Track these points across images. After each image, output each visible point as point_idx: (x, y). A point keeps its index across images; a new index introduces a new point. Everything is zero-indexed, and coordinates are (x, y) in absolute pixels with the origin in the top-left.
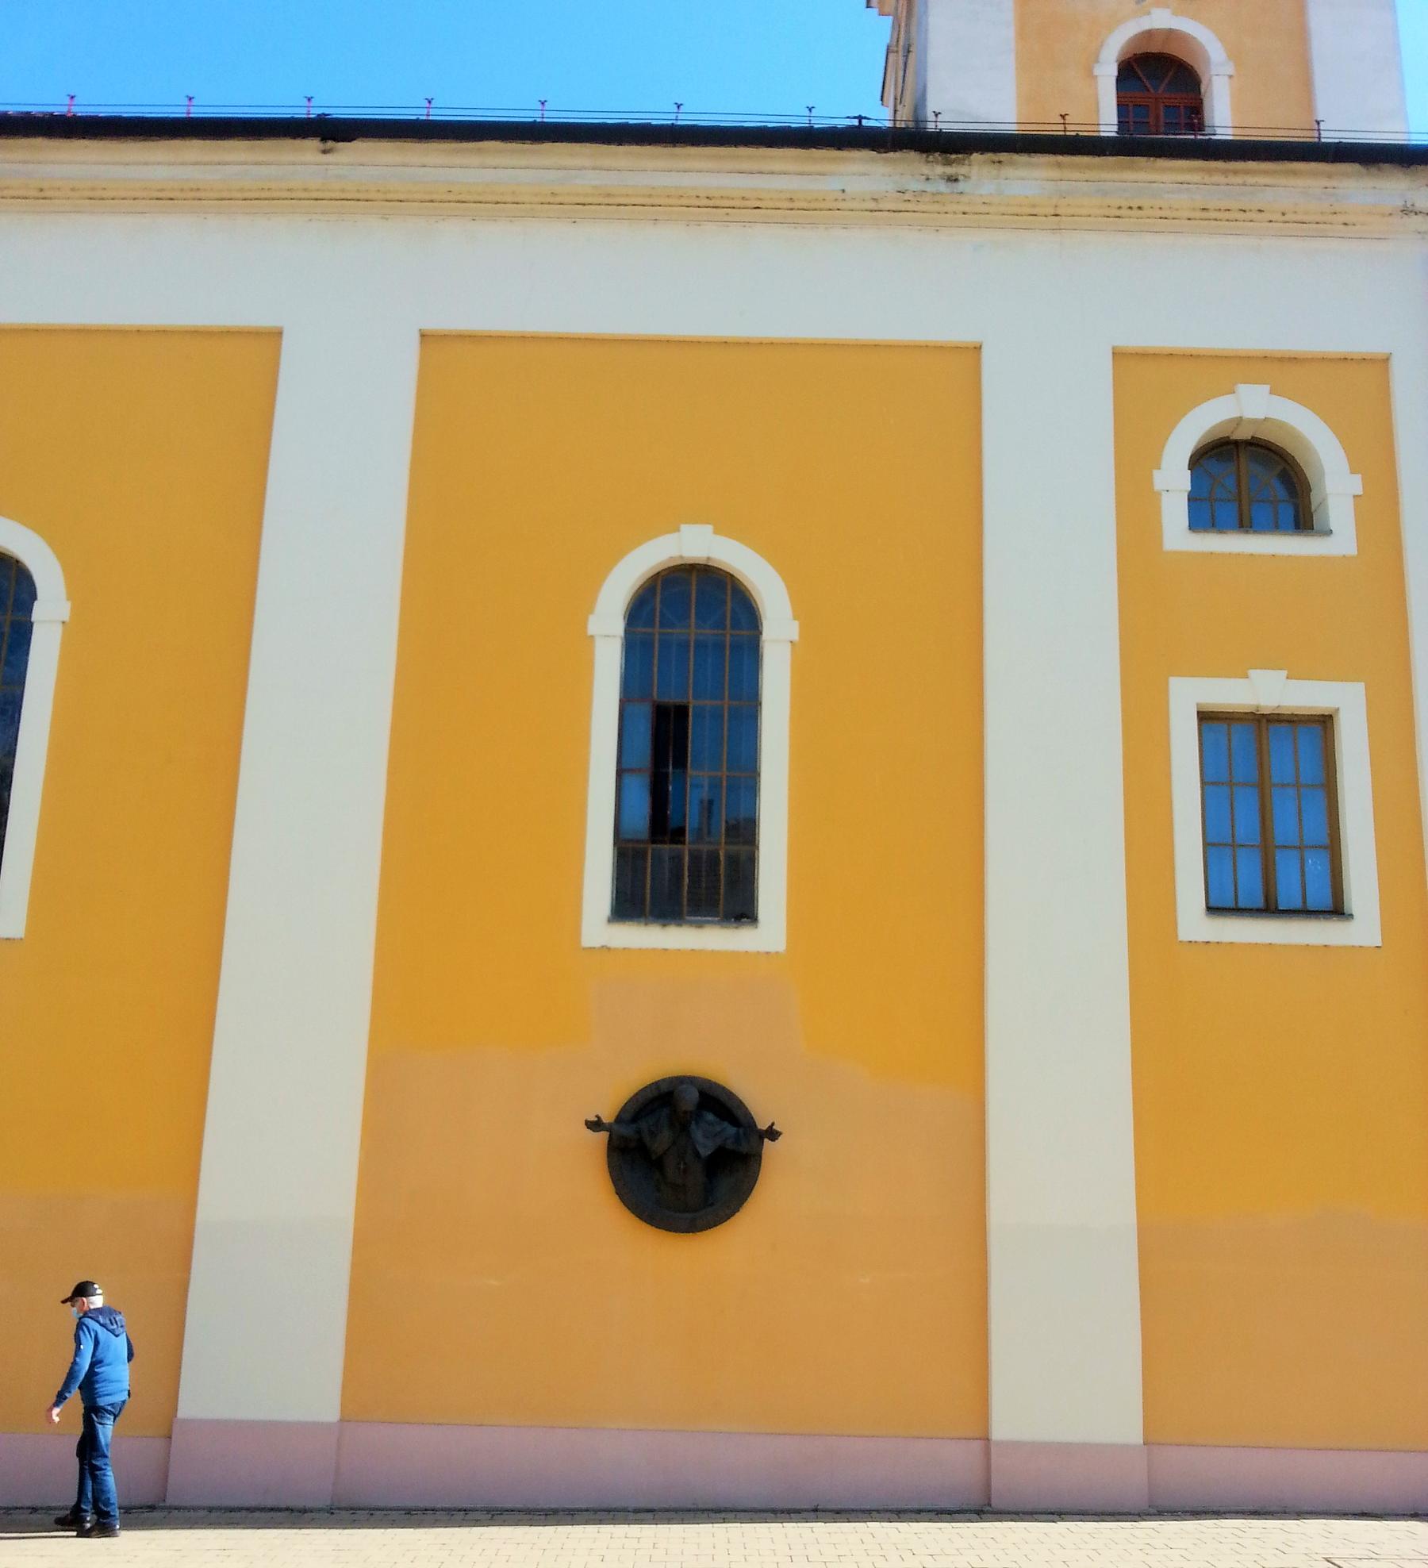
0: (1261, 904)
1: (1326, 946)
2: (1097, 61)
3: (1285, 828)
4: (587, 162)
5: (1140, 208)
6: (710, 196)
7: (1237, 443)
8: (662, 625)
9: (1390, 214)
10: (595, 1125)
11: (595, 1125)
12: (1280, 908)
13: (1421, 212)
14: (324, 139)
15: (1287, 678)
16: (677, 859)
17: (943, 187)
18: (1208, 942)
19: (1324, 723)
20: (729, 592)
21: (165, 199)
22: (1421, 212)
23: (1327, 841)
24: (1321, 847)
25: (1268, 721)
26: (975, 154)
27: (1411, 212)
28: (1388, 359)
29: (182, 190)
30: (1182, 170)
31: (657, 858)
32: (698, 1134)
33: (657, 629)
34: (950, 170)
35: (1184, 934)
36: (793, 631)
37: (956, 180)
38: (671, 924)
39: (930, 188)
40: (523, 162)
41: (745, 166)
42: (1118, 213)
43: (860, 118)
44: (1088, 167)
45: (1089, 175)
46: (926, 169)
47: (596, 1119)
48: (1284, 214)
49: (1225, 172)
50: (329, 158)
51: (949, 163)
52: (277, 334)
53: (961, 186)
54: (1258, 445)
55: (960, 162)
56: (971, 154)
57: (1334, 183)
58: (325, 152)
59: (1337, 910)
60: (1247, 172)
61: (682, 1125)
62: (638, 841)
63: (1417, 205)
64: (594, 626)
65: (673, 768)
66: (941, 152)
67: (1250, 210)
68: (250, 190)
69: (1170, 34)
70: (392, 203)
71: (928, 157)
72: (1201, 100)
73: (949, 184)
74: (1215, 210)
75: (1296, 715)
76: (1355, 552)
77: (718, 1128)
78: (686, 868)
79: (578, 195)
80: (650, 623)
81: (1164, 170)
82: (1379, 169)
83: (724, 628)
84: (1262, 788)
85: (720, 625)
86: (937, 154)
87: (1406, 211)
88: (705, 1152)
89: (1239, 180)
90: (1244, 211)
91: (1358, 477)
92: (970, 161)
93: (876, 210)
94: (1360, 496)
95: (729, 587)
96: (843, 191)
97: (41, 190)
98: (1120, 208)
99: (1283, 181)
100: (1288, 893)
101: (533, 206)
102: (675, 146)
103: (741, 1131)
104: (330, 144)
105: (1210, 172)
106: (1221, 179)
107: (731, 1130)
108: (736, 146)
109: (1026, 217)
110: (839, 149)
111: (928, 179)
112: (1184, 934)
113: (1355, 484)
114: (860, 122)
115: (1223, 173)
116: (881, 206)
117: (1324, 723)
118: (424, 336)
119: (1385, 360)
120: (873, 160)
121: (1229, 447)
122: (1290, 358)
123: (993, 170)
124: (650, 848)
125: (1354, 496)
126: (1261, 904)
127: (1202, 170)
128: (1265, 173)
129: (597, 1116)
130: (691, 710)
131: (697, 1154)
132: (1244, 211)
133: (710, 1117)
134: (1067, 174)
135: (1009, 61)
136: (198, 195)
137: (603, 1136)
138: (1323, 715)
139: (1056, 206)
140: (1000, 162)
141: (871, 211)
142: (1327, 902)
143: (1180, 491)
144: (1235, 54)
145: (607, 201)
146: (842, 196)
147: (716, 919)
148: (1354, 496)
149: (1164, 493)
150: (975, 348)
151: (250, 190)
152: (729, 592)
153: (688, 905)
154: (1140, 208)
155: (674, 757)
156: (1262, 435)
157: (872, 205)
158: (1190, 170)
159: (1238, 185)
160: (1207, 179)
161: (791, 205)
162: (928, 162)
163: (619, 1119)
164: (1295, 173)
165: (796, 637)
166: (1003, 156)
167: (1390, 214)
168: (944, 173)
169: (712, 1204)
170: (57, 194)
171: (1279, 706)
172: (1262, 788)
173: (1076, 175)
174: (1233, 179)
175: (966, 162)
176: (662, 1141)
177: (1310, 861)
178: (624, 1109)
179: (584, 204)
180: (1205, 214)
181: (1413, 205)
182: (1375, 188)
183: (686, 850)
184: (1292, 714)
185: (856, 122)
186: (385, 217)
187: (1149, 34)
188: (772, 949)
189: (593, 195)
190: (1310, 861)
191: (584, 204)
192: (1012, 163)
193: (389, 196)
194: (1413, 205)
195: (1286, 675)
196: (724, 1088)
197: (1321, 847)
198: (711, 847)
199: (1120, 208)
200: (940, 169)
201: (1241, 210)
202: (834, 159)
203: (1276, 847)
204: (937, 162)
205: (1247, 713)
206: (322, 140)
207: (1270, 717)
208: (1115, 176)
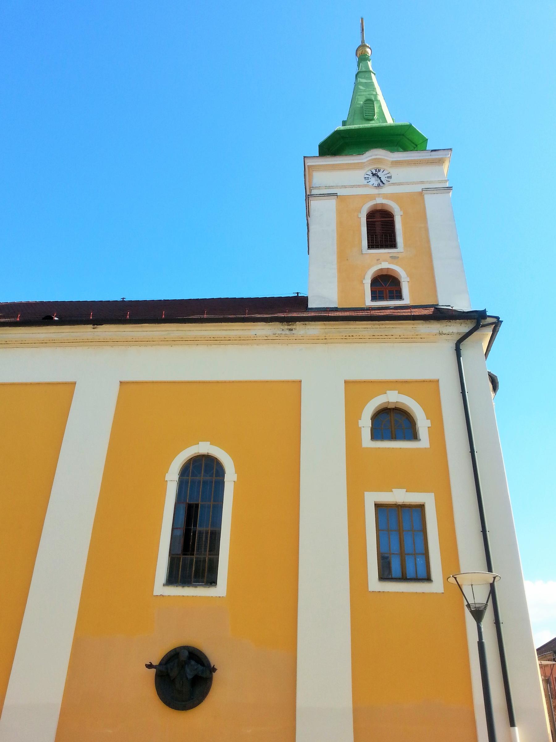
0: (400, 576)
1: (423, 593)
2: (364, 279)
3: (408, 547)
4: (175, 329)
5: (352, 336)
6: (214, 337)
7: (390, 409)
8: (192, 476)
9: (436, 335)
10: (150, 666)
11: (150, 666)
12: (408, 578)
13: (446, 334)
14: (94, 325)
15: (406, 492)
16: (192, 560)
17: (288, 332)
18: (380, 592)
19: (421, 507)
20: (215, 463)
21: (44, 343)
22: (446, 334)
23: (424, 552)
24: (422, 554)
25: (401, 507)
26: (297, 322)
27: (442, 334)
28: (438, 381)
29: (49, 340)
30: (364, 324)
31: (184, 560)
32: (188, 670)
33: (190, 478)
34: (289, 327)
35: (371, 589)
36: (235, 477)
37: (292, 330)
38: (185, 587)
39: (283, 333)
40: (155, 329)
41: (225, 328)
42: (346, 338)
43: (298, 293)
44: (334, 325)
45: (335, 327)
46: (282, 327)
47: (150, 664)
48: (400, 336)
49: (379, 325)
50: (95, 330)
51: (290, 325)
52: (74, 383)
53: (294, 332)
54: (397, 410)
55: (293, 325)
56: (296, 322)
57: (415, 326)
58: (94, 328)
59: (428, 579)
60: (385, 324)
61: (182, 666)
62: (177, 555)
63: (443, 332)
64: (168, 477)
65: (193, 527)
66: (286, 322)
67: (389, 335)
68: (70, 340)
69: (388, 269)
70: (114, 342)
71: (282, 323)
72: (401, 288)
73: (290, 331)
74: (377, 336)
75: (411, 505)
76: (429, 447)
77: (196, 667)
78: (194, 563)
79: (172, 338)
80: (188, 476)
81: (359, 325)
82: (429, 322)
83: (213, 477)
84: (400, 532)
85: (212, 476)
86: (285, 323)
87: (441, 334)
88: (190, 677)
89: (383, 326)
90: (387, 336)
91: (429, 421)
92: (296, 324)
93: (267, 339)
94: (430, 427)
95: (215, 461)
96: (256, 335)
97: (6, 342)
98: (346, 336)
99: (401, 326)
100: (410, 572)
101: (159, 342)
102: (202, 323)
103: (204, 668)
104: (95, 326)
105: (374, 325)
106: (378, 327)
107: (200, 667)
108: (221, 323)
109: (315, 340)
110: (254, 322)
111: (283, 330)
112: (371, 589)
113: (428, 423)
114: (298, 295)
115: (378, 325)
116: (269, 338)
117: (421, 507)
118: (121, 382)
119: (438, 381)
120: (265, 325)
121: (388, 411)
122: (405, 382)
123: (304, 327)
124: (182, 557)
125: (428, 427)
126: (400, 576)
127: (371, 324)
128: (392, 324)
129: (150, 663)
130: (199, 505)
131: (187, 678)
132: (387, 336)
133: (193, 662)
134: (327, 327)
135: (336, 280)
136: (54, 342)
137: (153, 671)
138: (421, 505)
139: (325, 336)
140: (305, 324)
141: (266, 340)
142: (424, 575)
143: (368, 427)
144: (409, 275)
145: (182, 340)
146: (255, 336)
147: (203, 584)
148: (428, 427)
149: (362, 428)
150: (300, 381)
151: (70, 340)
152: (215, 463)
153: (207, 572)
154: (352, 336)
155: (193, 524)
156: (399, 406)
157: (266, 338)
158: (367, 324)
159: (384, 328)
160: (373, 327)
161: (240, 339)
162: (282, 325)
163: (160, 664)
164: (402, 324)
165: (236, 480)
166: (307, 323)
167: (436, 335)
168: (288, 328)
169: (192, 699)
170: (11, 342)
171: (403, 502)
172: (400, 532)
173: (331, 327)
174: (381, 326)
175: (295, 324)
176: (174, 673)
177: (418, 559)
178: (162, 660)
179: (175, 341)
180: (374, 337)
181: (442, 332)
182: (429, 327)
183: (194, 557)
184: (410, 504)
185: (296, 295)
186: (112, 346)
187: (381, 270)
188: (221, 596)
189: (177, 338)
190: (418, 559)
191: (175, 341)
192: (309, 324)
193: (114, 341)
194: (442, 332)
195: (405, 491)
196: (200, 651)
197: (422, 554)
198: (204, 556)
199: (346, 336)
200: (286, 327)
201: (386, 335)
202: (252, 325)
203: (406, 554)
204: (285, 325)
205: (394, 504)
206: (93, 325)
207: (401, 506)
208: (343, 327)
